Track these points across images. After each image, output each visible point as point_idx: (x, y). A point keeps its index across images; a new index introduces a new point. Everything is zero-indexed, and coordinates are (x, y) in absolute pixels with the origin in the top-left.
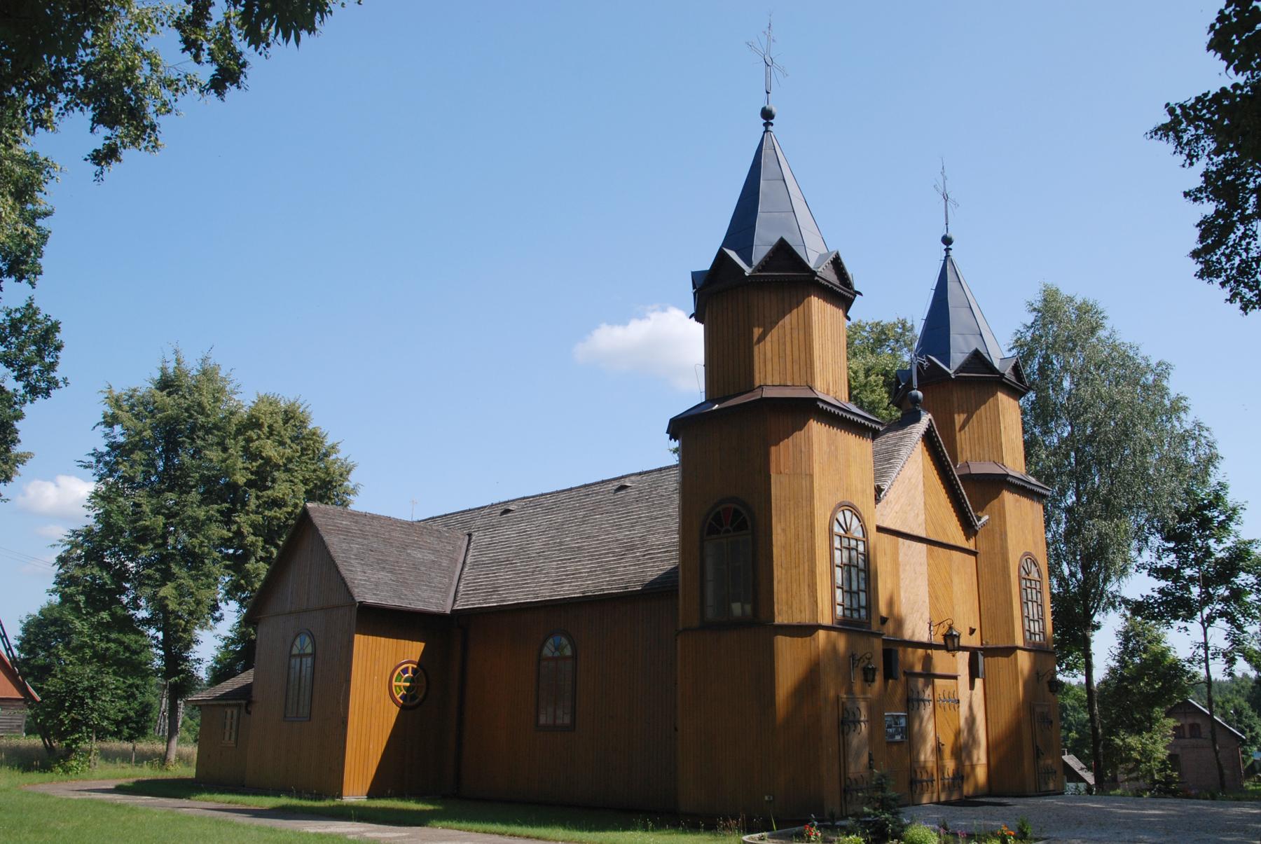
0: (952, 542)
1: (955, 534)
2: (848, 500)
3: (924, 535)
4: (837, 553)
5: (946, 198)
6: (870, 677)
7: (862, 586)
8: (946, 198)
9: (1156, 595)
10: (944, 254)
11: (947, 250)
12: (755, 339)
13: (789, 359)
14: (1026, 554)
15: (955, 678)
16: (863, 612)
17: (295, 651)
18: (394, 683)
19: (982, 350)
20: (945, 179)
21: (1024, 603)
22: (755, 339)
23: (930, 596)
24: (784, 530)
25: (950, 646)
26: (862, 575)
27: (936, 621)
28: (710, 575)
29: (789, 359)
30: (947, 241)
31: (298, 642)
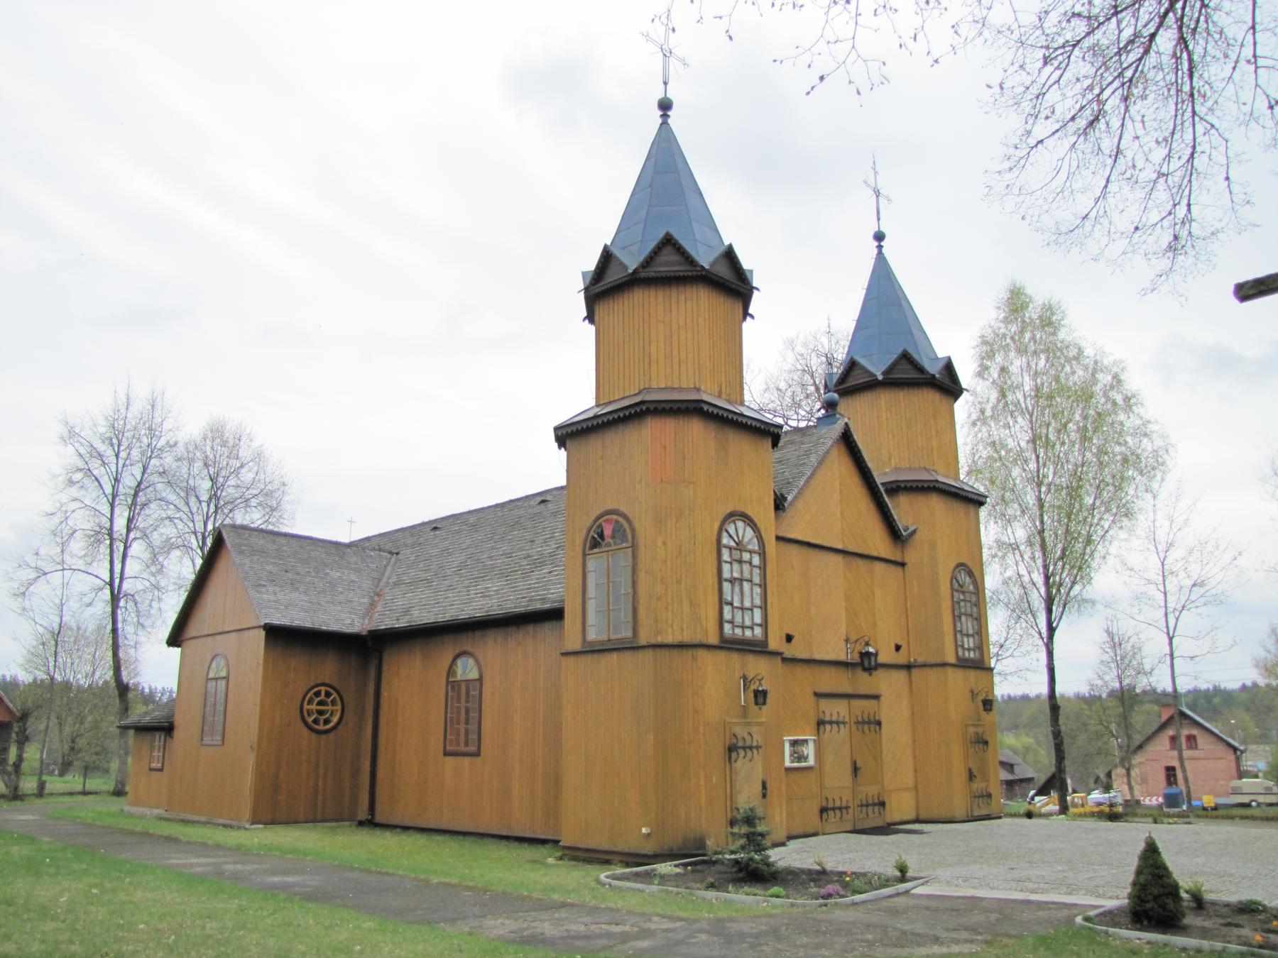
0: (875, 554)
1: (878, 542)
2: (741, 508)
3: (840, 546)
4: (726, 567)
5: (877, 193)
6: (761, 700)
7: (758, 602)
8: (877, 193)
9: (147, 690)
10: (876, 251)
11: (880, 247)
12: (921, 376)
13: (675, 360)
14: (961, 565)
15: (876, 697)
16: (758, 631)
17: (211, 675)
18: (306, 707)
19: (911, 351)
20: (876, 173)
21: (956, 618)
22: (921, 376)
23: (847, 611)
24: (665, 543)
25: (866, 664)
26: (758, 590)
27: (853, 638)
28: (591, 591)
29: (675, 360)
30: (879, 237)
31: (214, 665)
